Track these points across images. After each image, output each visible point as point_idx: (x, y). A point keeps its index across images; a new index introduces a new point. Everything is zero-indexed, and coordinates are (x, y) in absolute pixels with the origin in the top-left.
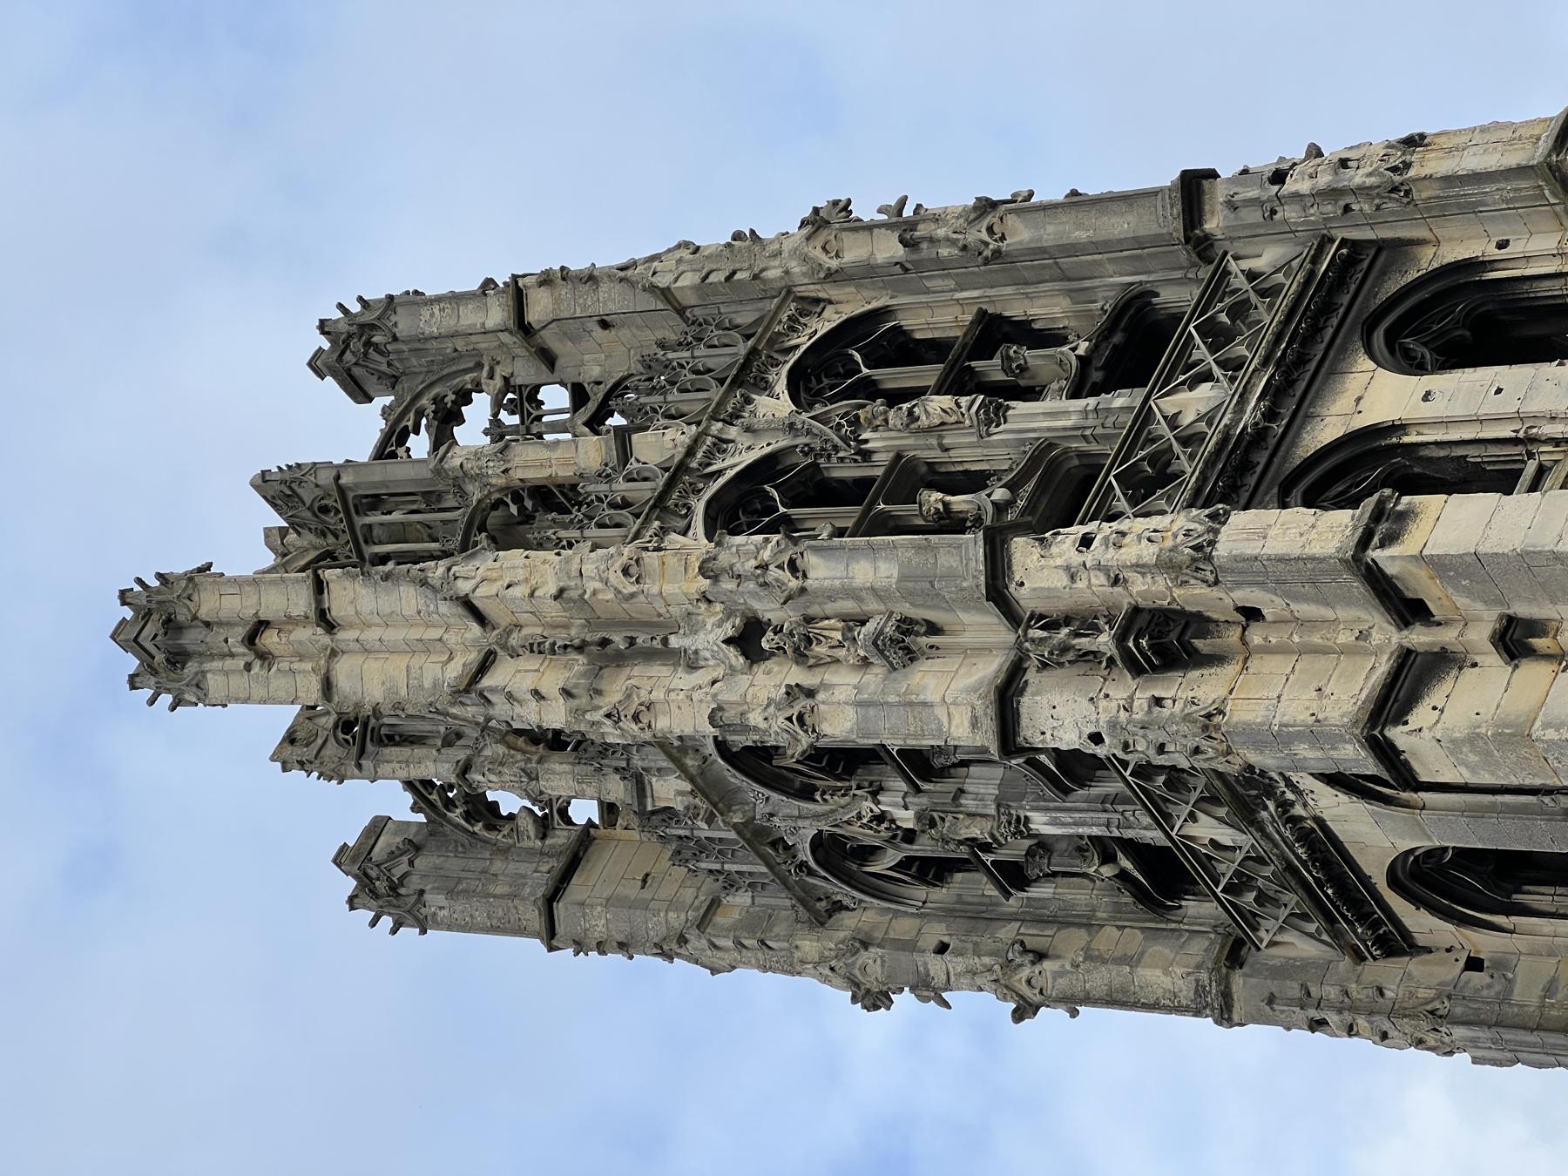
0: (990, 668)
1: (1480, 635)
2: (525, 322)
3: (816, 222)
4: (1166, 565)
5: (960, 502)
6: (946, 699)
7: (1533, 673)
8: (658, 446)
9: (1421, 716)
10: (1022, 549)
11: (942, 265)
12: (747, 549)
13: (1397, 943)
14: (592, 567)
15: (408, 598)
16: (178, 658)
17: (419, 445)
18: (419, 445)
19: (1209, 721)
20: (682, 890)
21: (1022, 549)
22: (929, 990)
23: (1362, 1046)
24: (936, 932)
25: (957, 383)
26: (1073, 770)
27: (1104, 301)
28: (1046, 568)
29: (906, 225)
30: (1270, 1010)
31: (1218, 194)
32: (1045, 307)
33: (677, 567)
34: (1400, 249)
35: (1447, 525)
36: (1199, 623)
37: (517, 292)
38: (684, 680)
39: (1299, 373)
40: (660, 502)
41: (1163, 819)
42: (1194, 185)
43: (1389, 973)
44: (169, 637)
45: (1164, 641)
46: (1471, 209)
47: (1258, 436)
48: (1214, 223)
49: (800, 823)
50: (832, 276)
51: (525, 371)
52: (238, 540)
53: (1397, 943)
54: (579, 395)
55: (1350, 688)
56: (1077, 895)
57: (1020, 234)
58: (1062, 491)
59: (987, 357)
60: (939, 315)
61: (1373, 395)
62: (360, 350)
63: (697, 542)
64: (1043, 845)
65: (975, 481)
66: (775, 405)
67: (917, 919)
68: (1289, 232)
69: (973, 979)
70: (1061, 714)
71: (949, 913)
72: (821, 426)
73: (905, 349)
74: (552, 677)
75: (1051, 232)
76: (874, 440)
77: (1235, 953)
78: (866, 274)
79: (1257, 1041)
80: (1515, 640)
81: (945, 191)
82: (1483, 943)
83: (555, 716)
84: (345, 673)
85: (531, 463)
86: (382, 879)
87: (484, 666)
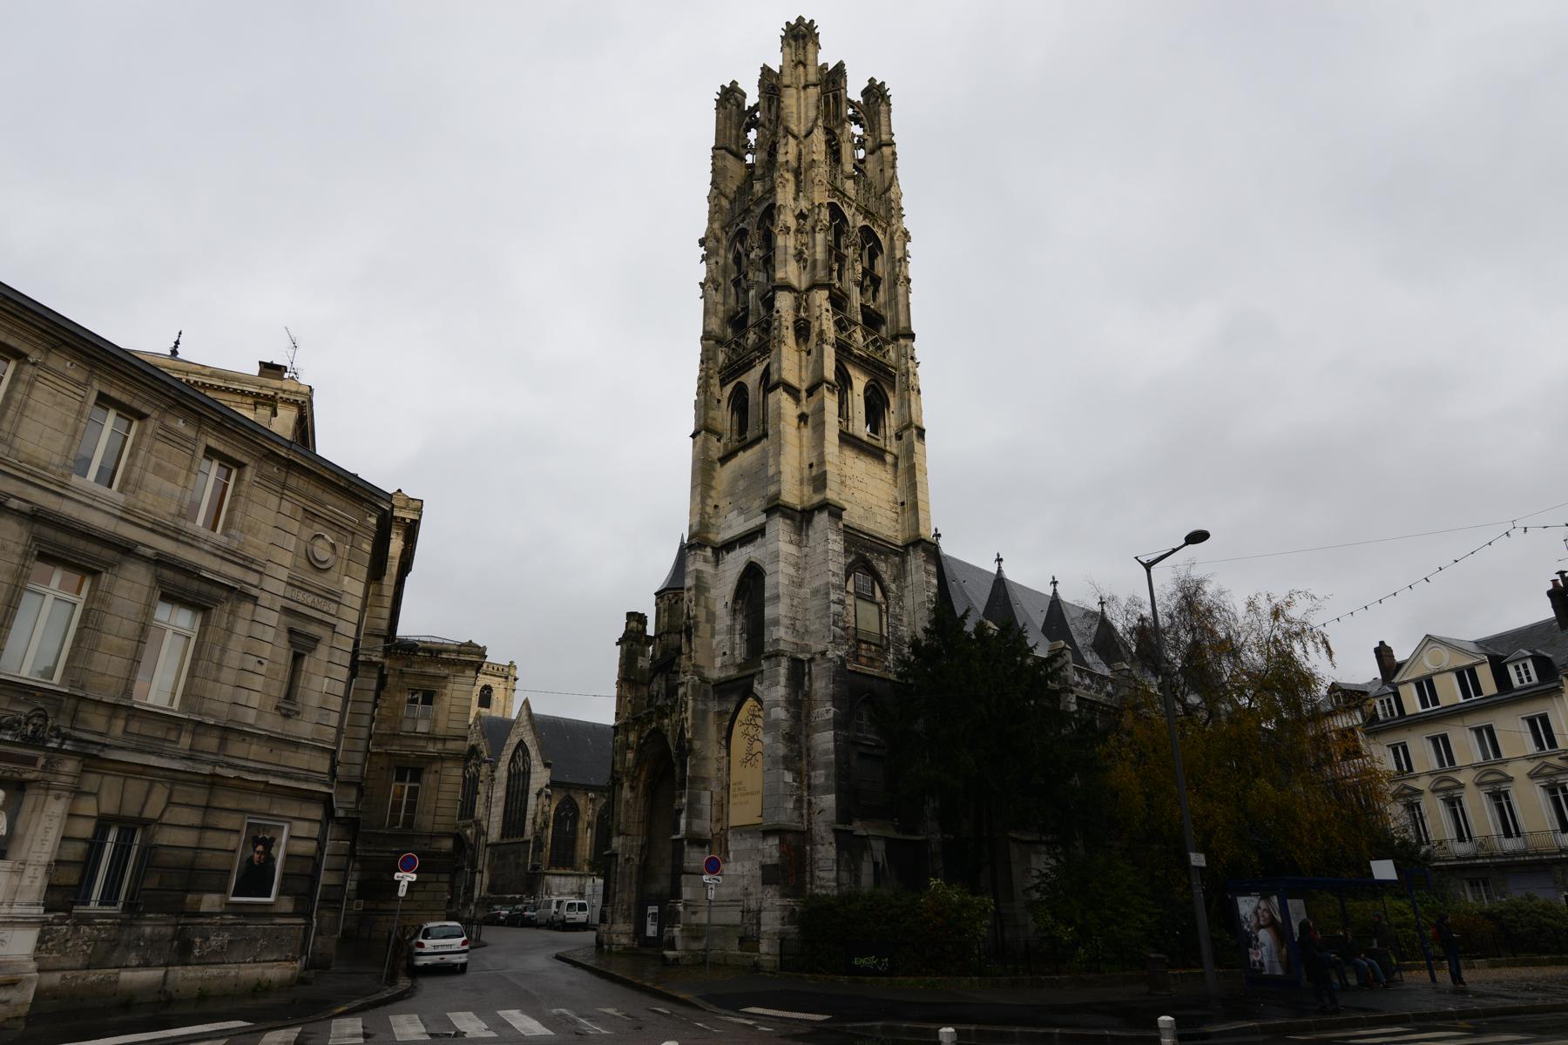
0: (795, 283)
1: (805, 409)
2: (881, 146)
3: (906, 234)
4: (821, 332)
5: (835, 274)
6: (789, 271)
7: (796, 421)
8: (849, 186)
9: (785, 395)
10: (825, 293)
11: (893, 268)
12: (825, 215)
13: (723, 383)
14: (822, 172)
15: (812, 113)
16: (796, 38)
17: (850, 111)
18: (850, 111)
19: (781, 342)
20: (731, 187)
21: (825, 293)
22: (704, 258)
23: (697, 373)
24: (721, 262)
25: (865, 273)
26: (769, 303)
27: (883, 312)
28: (821, 298)
29: (904, 258)
30: (705, 351)
31: (908, 342)
32: (882, 296)
33: (821, 196)
34: (893, 388)
35: (831, 403)
36: (807, 340)
37: (891, 144)
38: (791, 196)
39: (865, 364)
40: (837, 189)
41: (754, 326)
42: (912, 336)
43: (716, 381)
44: (800, 35)
45: (802, 330)
46: (902, 405)
47: (851, 353)
48: (902, 341)
49: (750, 224)
50: (892, 239)
51: (869, 144)
52: (827, 56)
53: (723, 383)
54: (862, 161)
55: (792, 379)
56: (732, 301)
57: (901, 290)
58: (839, 302)
59: (871, 281)
60: (881, 267)
61: (859, 382)
62: (876, 93)
63: (827, 200)
64: (746, 292)
65: (840, 279)
66: (860, 221)
67: (725, 256)
68: (898, 360)
69: (709, 271)
70: (784, 302)
71: (726, 265)
72: (855, 235)
73: (873, 257)
74: (791, 157)
75: (901, 299)
76: (851, 250)
77: (720, 342)
78: (892, 248)
79: (697, 349)
80: (803, 418)
81: (914, 269)
82: (724, 403)
83: (781, 158)
84: (792, 91)
85: (846, 149)
86: (729, 96)
87: (794, 137)
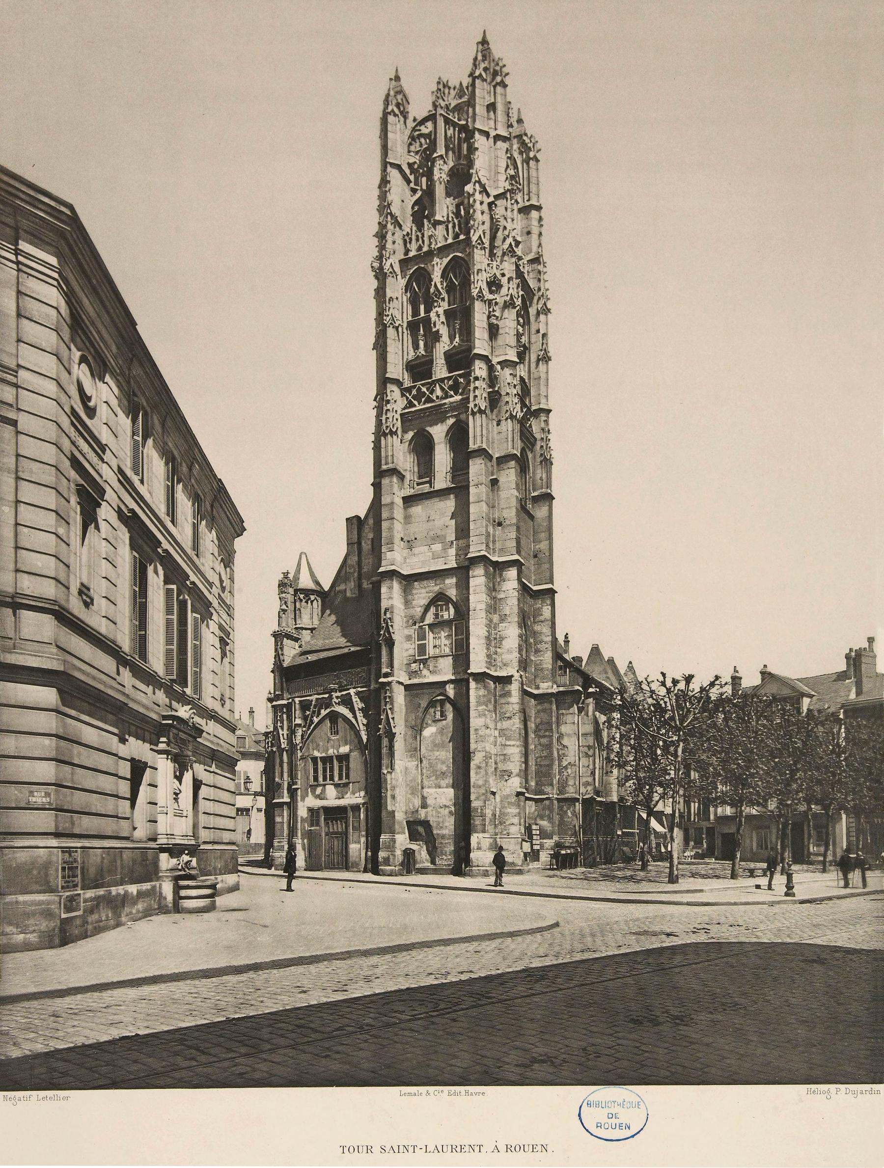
70: (480, 369)
